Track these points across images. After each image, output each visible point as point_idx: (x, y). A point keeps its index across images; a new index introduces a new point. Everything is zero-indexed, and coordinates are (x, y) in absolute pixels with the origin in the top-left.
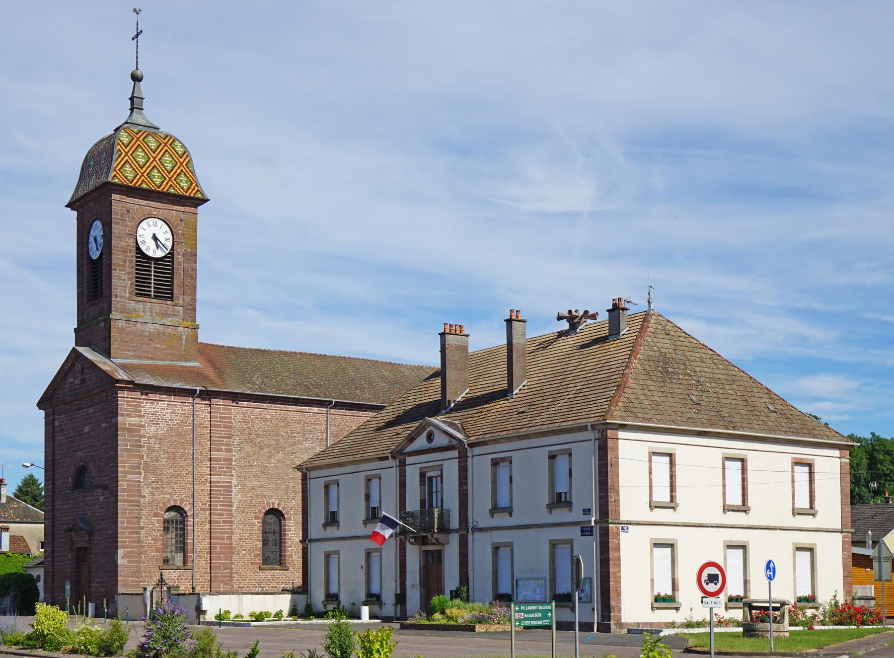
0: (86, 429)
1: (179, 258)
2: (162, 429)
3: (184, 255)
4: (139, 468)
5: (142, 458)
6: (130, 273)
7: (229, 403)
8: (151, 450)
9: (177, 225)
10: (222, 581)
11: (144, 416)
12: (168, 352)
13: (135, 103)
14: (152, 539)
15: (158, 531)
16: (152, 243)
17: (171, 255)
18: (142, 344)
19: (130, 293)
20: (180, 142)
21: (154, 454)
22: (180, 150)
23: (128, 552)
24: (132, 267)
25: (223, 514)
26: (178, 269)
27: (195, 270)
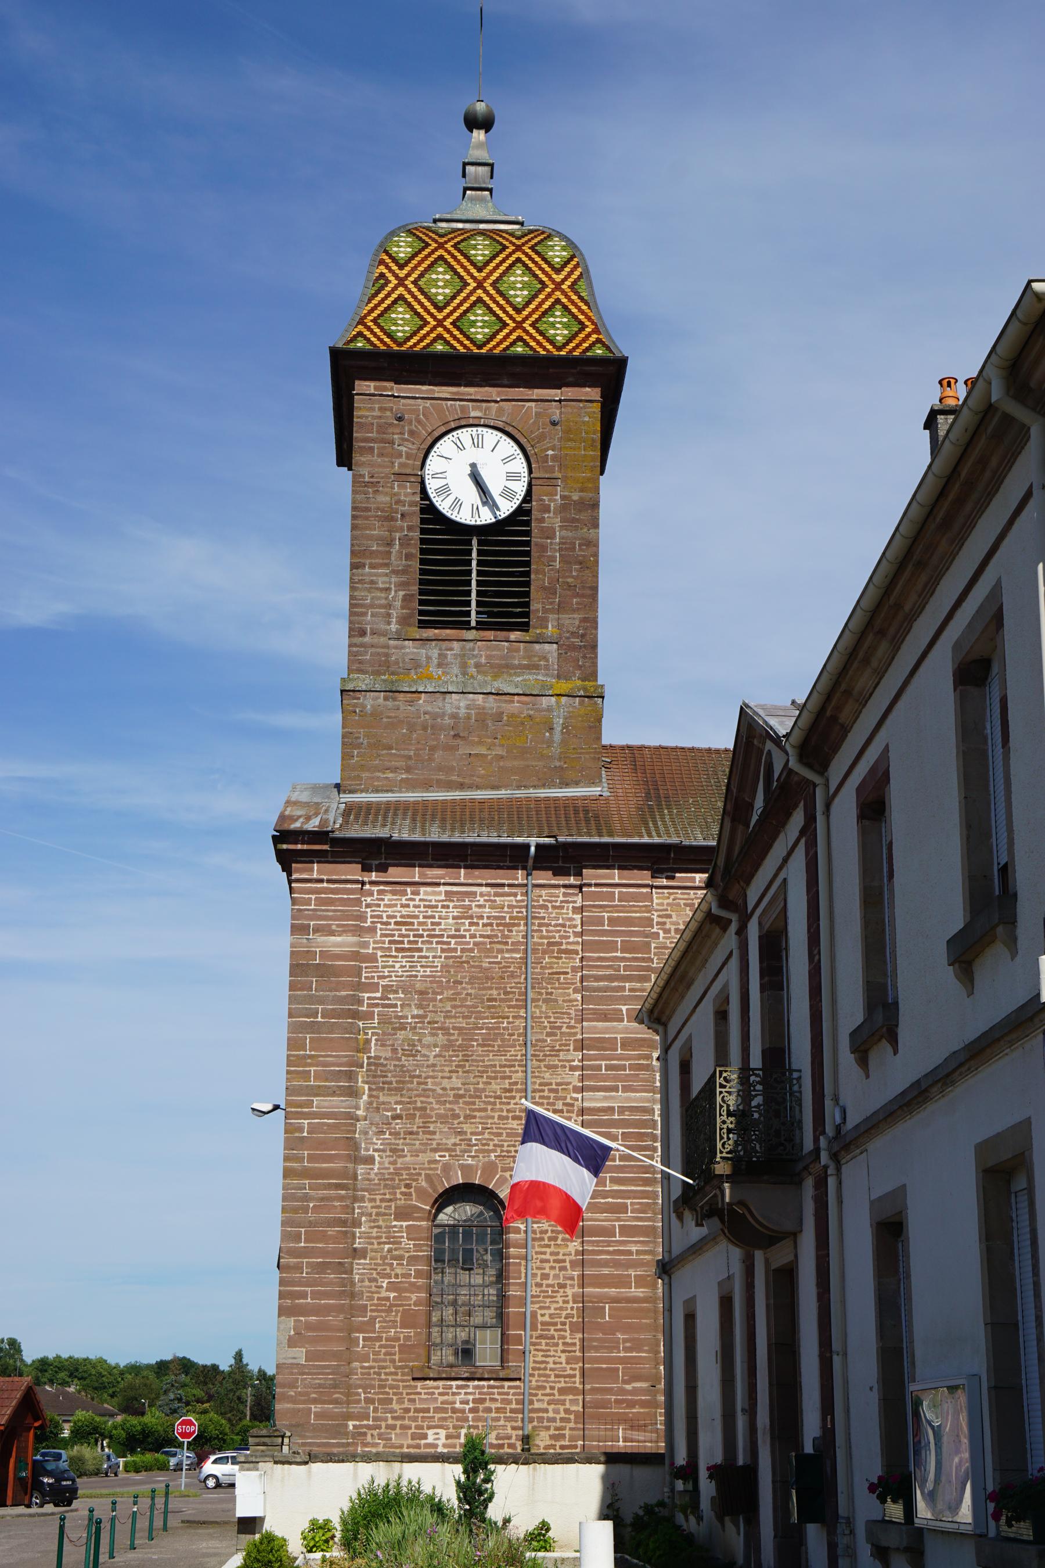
1: (549, 521)
2: (431, 962)
3: (563, 508)
4: (351, 1076)
5: (365, 1047)
6: (404, 572)
7: (644, 877)
8: (392, 1025)
9: (542, 437)
10: (622, 1419)
11: (372, 930)
12: (509, 764)
14: (392, 1287)
15: (413, 1260)
16: (470, 494)
17: (521, 515)
18: (433, 749)
19: (403, 621)
20: (563, 237)
21: (401, 1035)
22: (557, 253)
23: (309, 1327)
24: (408, 557)
25: (623, 1208)
26: (543, 548)
27: (592, 544)
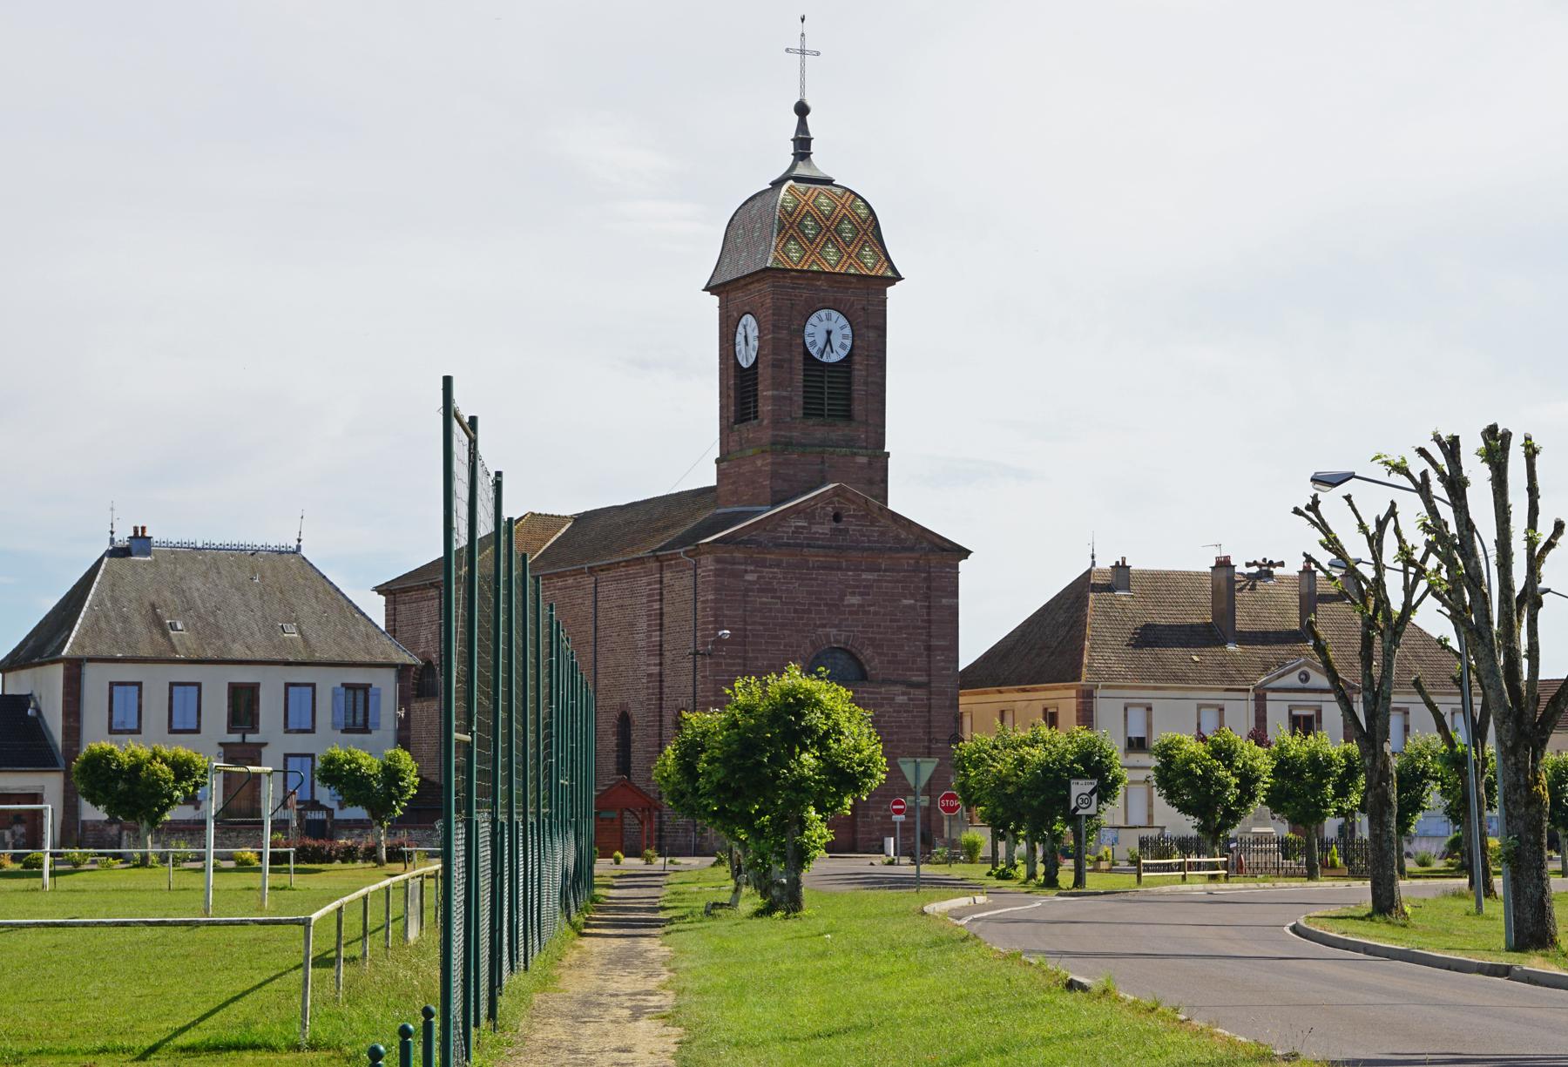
0: (856, 600)
1: (859, 371)
13: (802, 146)
